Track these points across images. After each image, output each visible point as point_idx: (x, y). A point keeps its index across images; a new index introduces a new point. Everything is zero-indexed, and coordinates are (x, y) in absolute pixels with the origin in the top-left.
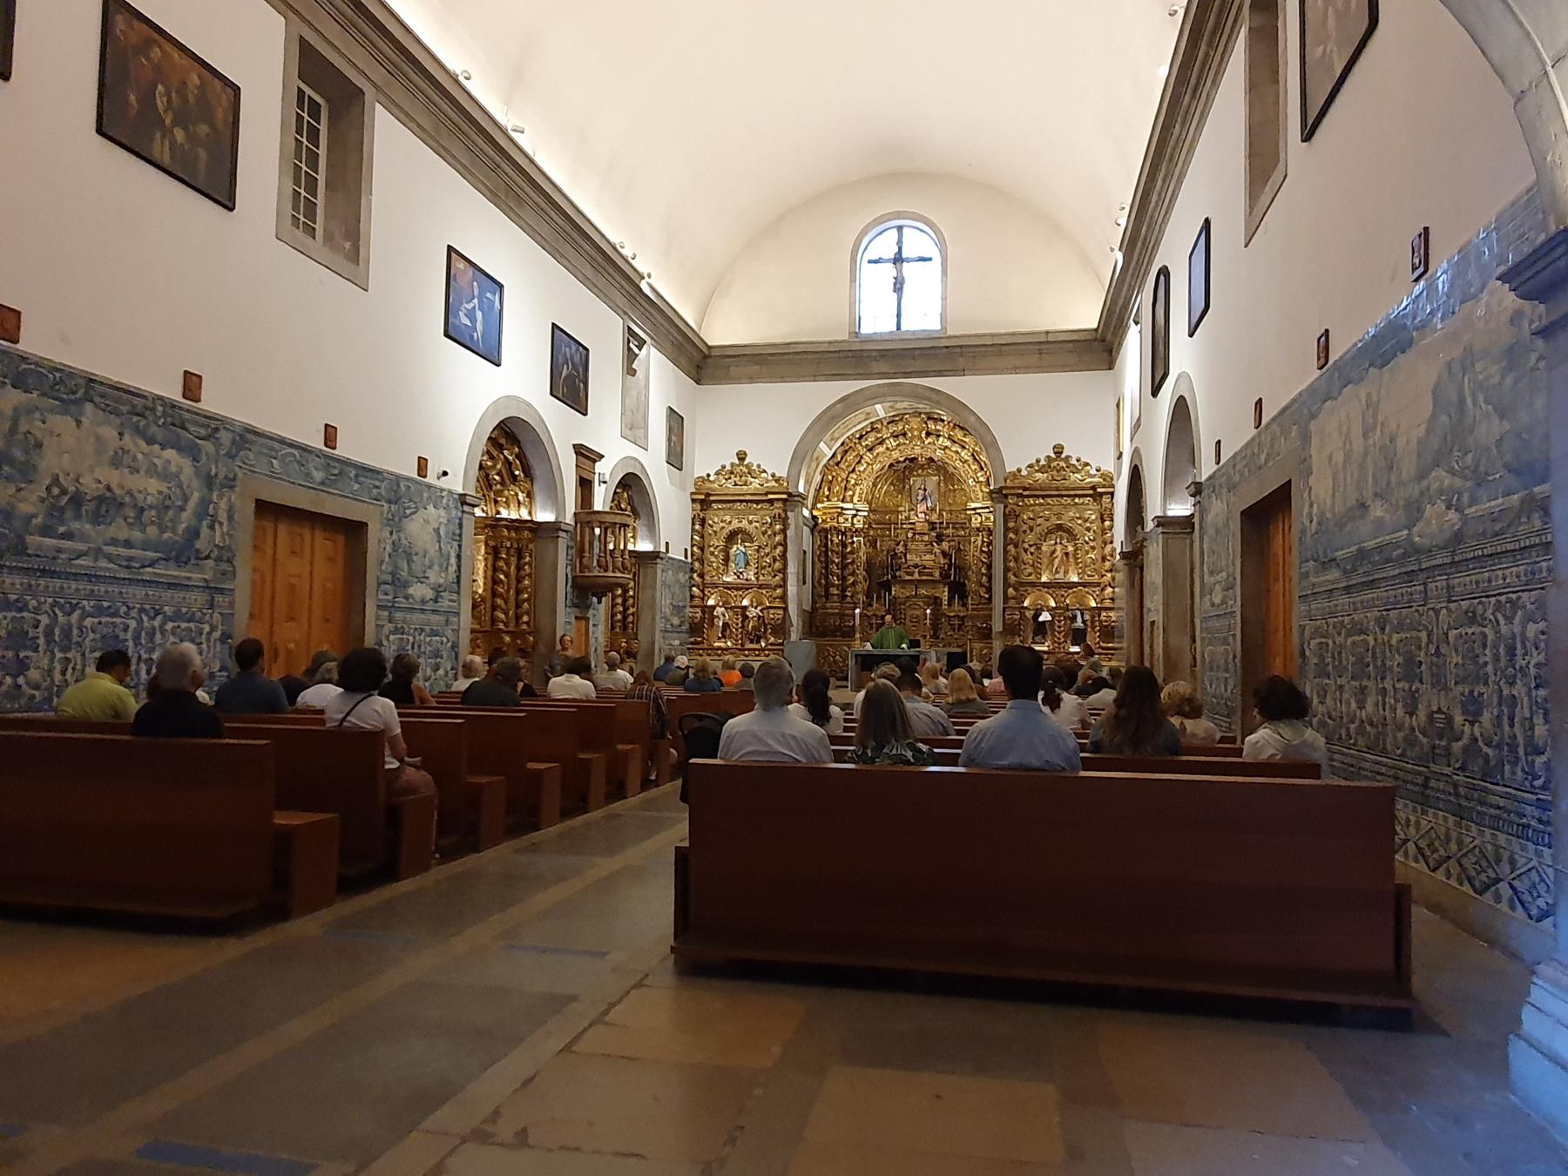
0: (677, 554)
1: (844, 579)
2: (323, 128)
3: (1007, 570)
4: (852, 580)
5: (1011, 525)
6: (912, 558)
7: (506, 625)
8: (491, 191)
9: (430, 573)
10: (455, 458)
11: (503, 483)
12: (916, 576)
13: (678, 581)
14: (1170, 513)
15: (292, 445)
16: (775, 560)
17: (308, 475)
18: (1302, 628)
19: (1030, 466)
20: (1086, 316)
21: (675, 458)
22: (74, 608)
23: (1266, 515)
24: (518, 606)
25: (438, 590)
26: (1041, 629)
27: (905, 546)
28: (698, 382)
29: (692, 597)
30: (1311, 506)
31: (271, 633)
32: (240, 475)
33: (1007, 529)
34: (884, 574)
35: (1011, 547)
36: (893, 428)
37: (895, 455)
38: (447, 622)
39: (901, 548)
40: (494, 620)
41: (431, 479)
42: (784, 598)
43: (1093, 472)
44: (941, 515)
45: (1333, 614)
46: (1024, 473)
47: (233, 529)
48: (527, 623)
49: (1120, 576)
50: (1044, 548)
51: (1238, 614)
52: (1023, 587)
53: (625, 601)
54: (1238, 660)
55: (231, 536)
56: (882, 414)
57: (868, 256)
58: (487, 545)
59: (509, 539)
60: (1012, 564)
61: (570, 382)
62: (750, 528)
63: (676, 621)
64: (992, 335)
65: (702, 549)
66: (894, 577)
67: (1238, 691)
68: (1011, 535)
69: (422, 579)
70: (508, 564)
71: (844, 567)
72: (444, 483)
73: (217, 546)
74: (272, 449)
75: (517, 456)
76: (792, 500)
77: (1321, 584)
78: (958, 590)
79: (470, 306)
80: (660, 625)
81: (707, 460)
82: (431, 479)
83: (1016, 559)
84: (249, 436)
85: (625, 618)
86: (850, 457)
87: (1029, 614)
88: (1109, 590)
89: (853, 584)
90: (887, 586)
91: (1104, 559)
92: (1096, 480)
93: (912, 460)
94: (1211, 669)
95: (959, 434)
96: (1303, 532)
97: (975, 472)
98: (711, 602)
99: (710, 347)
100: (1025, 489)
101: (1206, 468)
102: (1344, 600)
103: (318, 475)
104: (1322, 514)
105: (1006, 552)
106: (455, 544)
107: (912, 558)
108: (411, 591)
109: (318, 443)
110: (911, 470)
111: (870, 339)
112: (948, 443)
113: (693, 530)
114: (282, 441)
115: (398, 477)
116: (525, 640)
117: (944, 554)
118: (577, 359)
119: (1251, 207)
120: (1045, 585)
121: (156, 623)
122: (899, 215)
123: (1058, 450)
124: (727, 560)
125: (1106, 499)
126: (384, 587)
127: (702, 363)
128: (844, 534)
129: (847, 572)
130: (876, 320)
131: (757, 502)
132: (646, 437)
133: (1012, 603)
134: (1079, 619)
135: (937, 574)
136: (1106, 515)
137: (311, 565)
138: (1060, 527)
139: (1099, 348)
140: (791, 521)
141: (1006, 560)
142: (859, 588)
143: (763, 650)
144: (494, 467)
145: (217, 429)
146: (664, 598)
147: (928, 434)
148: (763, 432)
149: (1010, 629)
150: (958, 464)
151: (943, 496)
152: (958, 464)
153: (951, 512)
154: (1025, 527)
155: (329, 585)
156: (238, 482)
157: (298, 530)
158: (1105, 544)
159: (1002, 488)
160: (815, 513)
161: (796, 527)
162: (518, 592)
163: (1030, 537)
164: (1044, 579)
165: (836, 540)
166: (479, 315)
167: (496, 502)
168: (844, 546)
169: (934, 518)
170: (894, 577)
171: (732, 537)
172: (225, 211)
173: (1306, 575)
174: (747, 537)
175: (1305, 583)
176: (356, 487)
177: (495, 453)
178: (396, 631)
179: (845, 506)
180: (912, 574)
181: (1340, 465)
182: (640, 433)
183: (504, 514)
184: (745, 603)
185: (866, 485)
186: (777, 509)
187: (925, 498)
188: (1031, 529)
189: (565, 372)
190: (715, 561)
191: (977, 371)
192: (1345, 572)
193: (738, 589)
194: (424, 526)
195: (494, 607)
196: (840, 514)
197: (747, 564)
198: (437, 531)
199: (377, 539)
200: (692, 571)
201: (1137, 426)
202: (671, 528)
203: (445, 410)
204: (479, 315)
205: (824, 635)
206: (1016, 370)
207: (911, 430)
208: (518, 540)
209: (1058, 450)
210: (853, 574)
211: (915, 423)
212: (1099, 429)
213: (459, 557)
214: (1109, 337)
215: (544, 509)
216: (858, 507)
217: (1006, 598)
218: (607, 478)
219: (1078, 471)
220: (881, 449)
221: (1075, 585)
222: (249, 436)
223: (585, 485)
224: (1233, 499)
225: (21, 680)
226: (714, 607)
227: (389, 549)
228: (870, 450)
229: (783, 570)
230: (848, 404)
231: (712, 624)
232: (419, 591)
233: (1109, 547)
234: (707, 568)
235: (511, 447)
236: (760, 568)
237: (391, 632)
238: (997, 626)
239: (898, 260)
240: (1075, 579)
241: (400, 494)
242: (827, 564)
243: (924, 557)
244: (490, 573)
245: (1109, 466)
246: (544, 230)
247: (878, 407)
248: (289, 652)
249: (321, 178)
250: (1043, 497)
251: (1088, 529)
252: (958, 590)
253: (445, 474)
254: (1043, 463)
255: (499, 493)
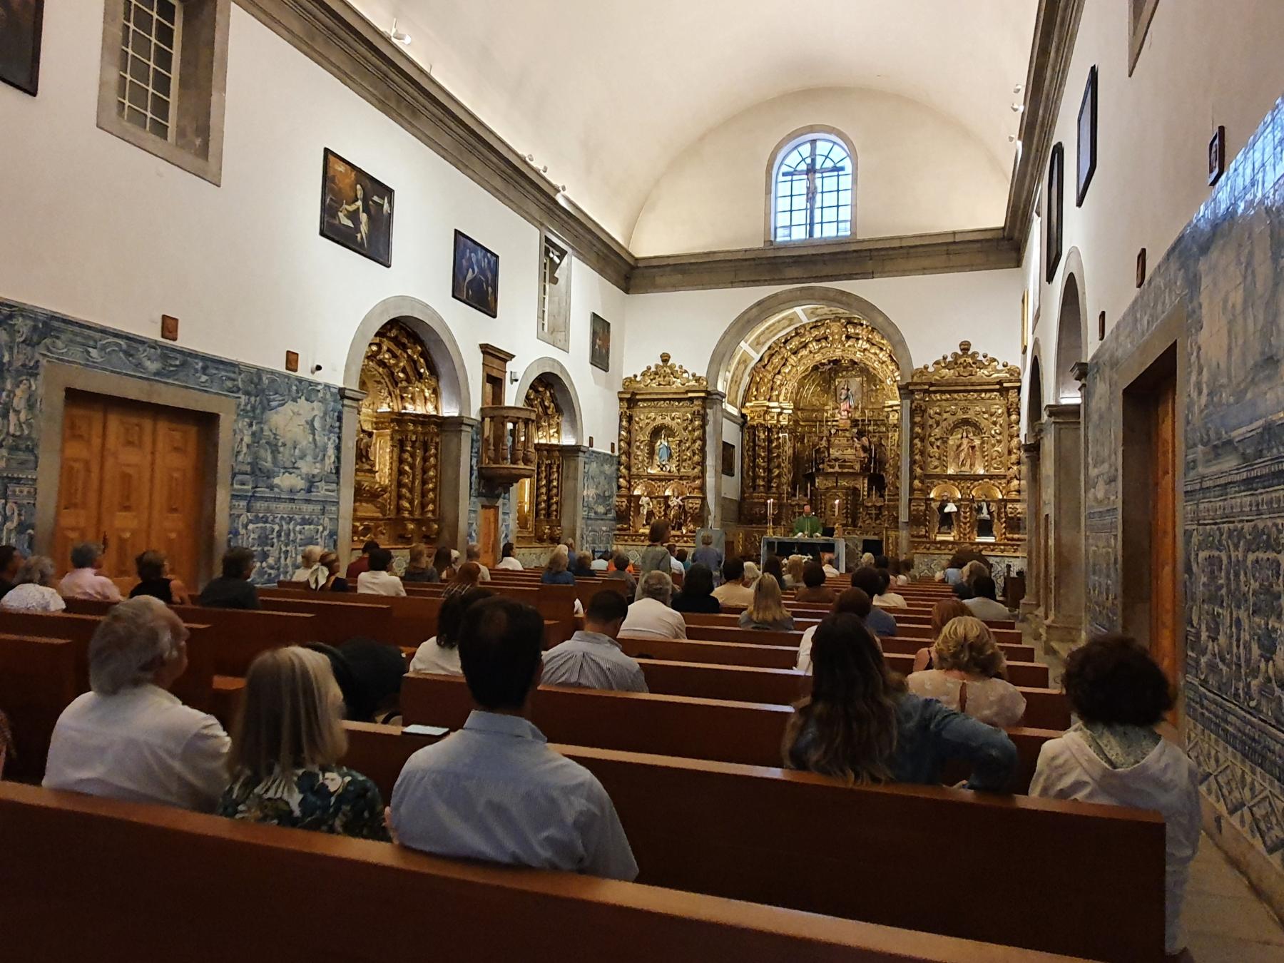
0: (602, 447)
1: (769, 471)
2: (177, 28)
3: (913, 462)
4: (776, 472)
5: (918, 419)
6: (834, 453)
7: (411, 513)
8: (380, 101)
9: (300, 464)
10: (334, 355)
11: (408, 380)
12: (837, 469)
13: (602, 472)
14: (1064, 402)
15: (117, 335)
16: (694, 454)
17: (139, 365)
18: (1189, 535)
19: (937, 363)
20: (994, 216)
21: (600, 358)
22: (291, 519)
23: (1151, 390)
24: (424, 494)
25: (311, 482)
26: (947, 520)
27: (829, 441)
28: (627, 291)
29: (619, 487)
30: (1200, 372)
31: (99, 521)
32: (44, 362)
33: (913, 424)
34: (807, 469)
35: (917, 441)
36: (815, 333)
37: (818, 357)
38: (323, 512)
39: (824, 443)
40: (399, 509)
41: (303, 372)
42: (702, 488)
43: (1000, 367)
44: (863, 412)
45: (1228, 518)
46: (931, 369)
47: (35, 417)
48: (433, 512)
49: (1024, 468)
50: (951, 442)
51: (1120, 510)
52: (929, 479)
53: (549, 490)
54: (1119, 566)
55: (30, 426)
56: (805, 320)
57: (784, 169)
58: (392, 439)
59: (415, 433)
60: (917, 457)
61: (476, 283)
62: (673, 424)
63: (601, 509)
64: (901, 238)
65: (629, 444)
66: (818, 470)
67: (1119, 602)
68: (918, 430)
69: (291, 469)
70: (413, 456)
71: (770, 460)
72: (319, 377)
73: (13, 435)
74: (90, 337)
75: (422, 355)
76: (710, 398)
77: (1210, 477)
78: (877, 482)
79: (351, 208)
80: (581, 512)
81: (633, 359)
82: (303, 372)
83: (922, 453)
84: (56, 324)
85: (549, 506)
86: (776, 360)
87: (935, 505)
88: (1016, 482)
89: (779, 476)
90: (811, 478)
91: (1010, 452)
92: (1002, 375)
93: (836, 362)
94: (1094, 573)
95: (877, 338)
96: (1189, 407)
97: (892, 371)
98: (637, 492)
99: (637, 259)
100: (931, 385)
101: (1092, 346)
102: (1242, 500)
103: (153, 366)
104: (1214, 377)
105: (912, 445)
106: (334, 437)
107: (834, 453)
108: (276, 481)
109: (154, 334)
110: (836, 372)
111: (785, 246)
112: (867, 346)
113: (621, 427)
114: (104, 331)
115: (260, 371)
116: (429, 528)
117: (864, 448)
118: (484, 264)
119: (1135, 28)
120: (950, 477)
121: (291, 527)
122: (812, 129)
123: (965, 347)
124: (652, 453)
125: (1012, 394)
126: (239, 477)
127: (629, 273)
128: (770, 430)
129: (772, 465)
130: (791, 228)
131: (679, 400)
132: (567, 341)
133: (917, 495)
134: (985, 510)
135: (858, 467)
136: (1012, 409)
137: (159, 458)
138: (966, 422)
139: (1003, 247)
140: (710, 418)
141: (912, 453)
142: (784, 480)
143: (683, 536)
144: (396, 365)
145: (11, 317)
146: (587, 488)
147: (848, 337)
148: (681, 335)
149: (916, 520)
150: (876, 365)
151: (866, 395)
152: (876, 365)
153: (873, 410)
154: (931, 422)
155: (176, 475)
156: (41, 371)
157: (134, 420)
158: (1012, 437)
159: (909, 384)
160: (744, 411)
161: (715, 422)
162: (424, 482)
163: (937, 432)
164: (950, 471)
165: (762, 436)
166: (364, 217)
167: (402, 398)
168: (770, 441)
169: (857, 415)
170: (818, 470)
171: (656, 433)
172: (31, 97)
173: (1191, 465)
174: (670, 433)
175: (1192, 474)
176: (204, 378)
177: (399, 352)
178: (257, 520)
179: (772, 404)
180: (832, 467)
181: (1239, 308)
182: (561, 336)
183: (410, 409)
184: (668, 493)
185: (792, 385)
186: (697, 406)
187: (847, 397)
188: (938, 424)
189: (470, 276)
190: (641, 454)
191: (884, 273)
192: (1245, 457)
193: (661, 480)
194: (291, 420)
195: (400, 497)
196: (766, 412)
197: (670, 456)
198: (311, 423)
199: (233, 433)
200: (619, 463)
201: (1037, 317)
202: (596, 420)
203: (326, 312)
204: (364, 217)
205: (751, 522)
206: (924, 270)
207: (832, 334)
208: (424, 434)
209: (965, 347)
210: (779, 467)
211: (835, 327)
212: (999, 325)
213: (338, 448)
214: (1016, 234)
215: (449, 404)
216: (784, 405)
217: (912, 490)
218: (519, 376)
219: (985, 367)
220: (804, 352)
221: (982, 477)
222: (56, 324)
223: (495, 382)
224: (1115, 377)
225: (264, 564)
226: (639, 497)
227: (247, 439)
228: (795, 353)
229: (702, 463)
230: (763, 309)
231: (638, 512)
232: (284, 481)
233: (1015, 440)
234: (633, 461)
235: (405, 344)
236: (681, 461)
237: (251, 521)
238: (904, 518)
239: (811, 170)
240: (981, 472)
241: (260, 390)
242: (755, 456)
243: (846, 451)
244: (395, 465)
245: (1016, 361)
246: (446, 141)
247: (798, 310)
248: (122, 541)
249: (175, 76)
250: (950, 392)
251: (995, 423)
252: (877, 482)
253: (319, 368)
254: (949, 359)
255: (404, 390)
